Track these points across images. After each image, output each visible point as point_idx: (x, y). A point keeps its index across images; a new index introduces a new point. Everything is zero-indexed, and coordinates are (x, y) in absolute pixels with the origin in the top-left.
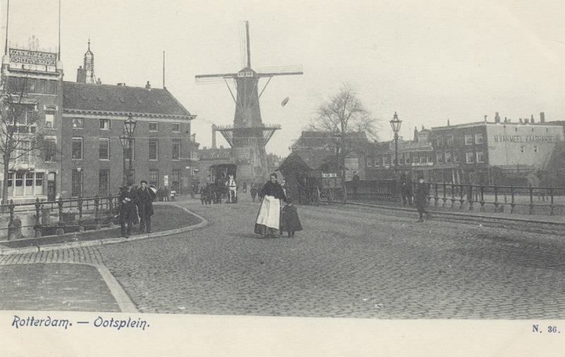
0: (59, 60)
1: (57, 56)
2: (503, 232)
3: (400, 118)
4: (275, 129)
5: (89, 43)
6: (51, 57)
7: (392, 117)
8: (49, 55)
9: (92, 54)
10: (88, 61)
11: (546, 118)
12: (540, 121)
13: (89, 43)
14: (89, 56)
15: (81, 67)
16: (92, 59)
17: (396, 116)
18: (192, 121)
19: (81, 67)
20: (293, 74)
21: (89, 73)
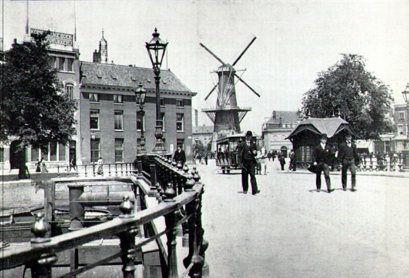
0: (75, 40)
1: (73, 37)
2: (221, 141)
3: (163, 39)
4: (247, 111)
5: (103, 32)
6: (68, 37)
7: (150, 39)
8: (67, 36)
9: (106, 42)
10: (103, 48)
11: (340, 177)
12: (358, 147)
13: (103, 32)
14: (103, 44)
15: (96, 50)
16: (106, 46)
17: (156, 35)
18: (193, 97)
19: (96, 50)
20: (211, 53)
21: (103, 58)
